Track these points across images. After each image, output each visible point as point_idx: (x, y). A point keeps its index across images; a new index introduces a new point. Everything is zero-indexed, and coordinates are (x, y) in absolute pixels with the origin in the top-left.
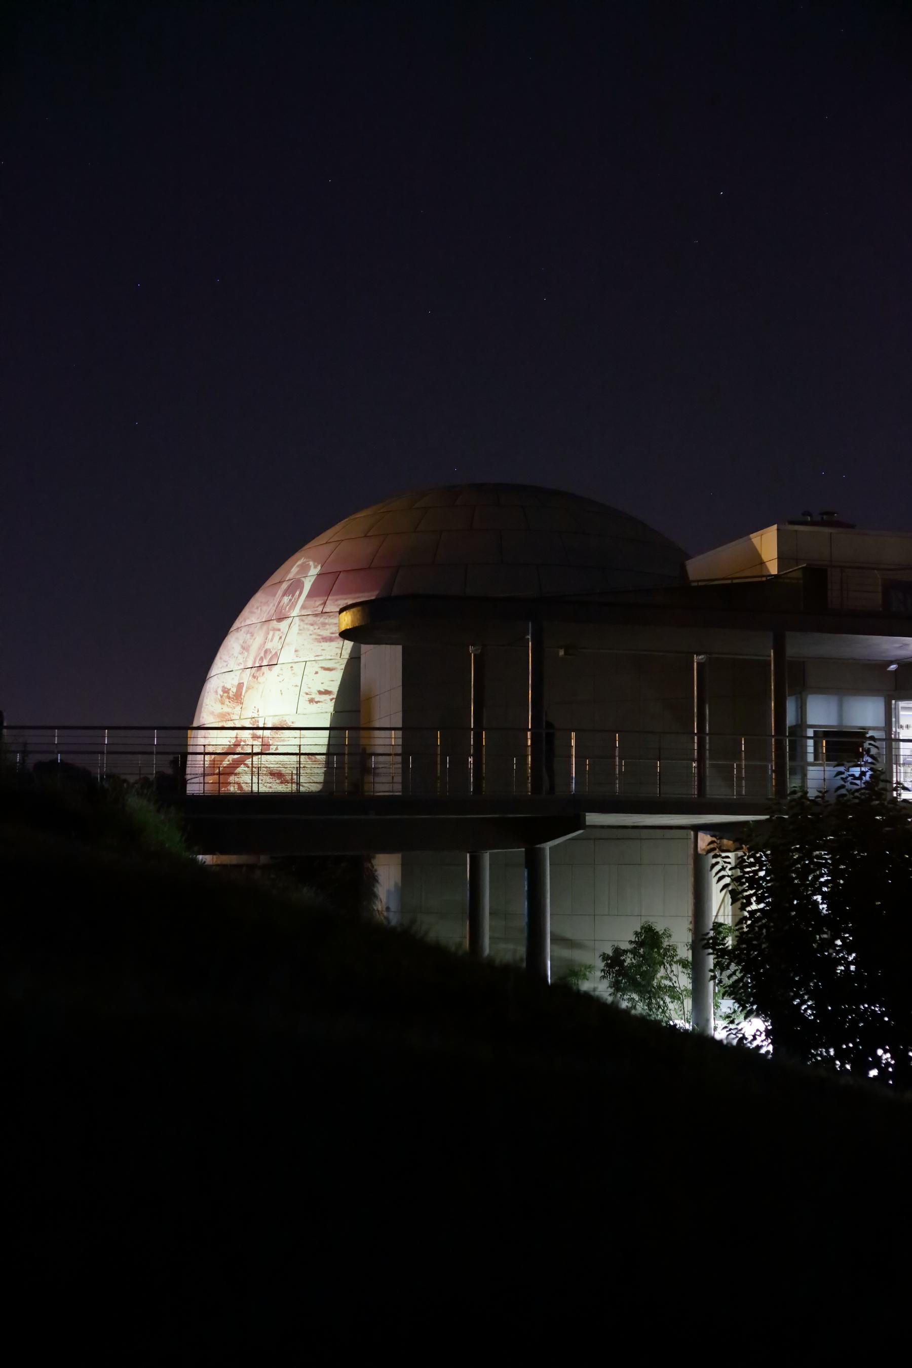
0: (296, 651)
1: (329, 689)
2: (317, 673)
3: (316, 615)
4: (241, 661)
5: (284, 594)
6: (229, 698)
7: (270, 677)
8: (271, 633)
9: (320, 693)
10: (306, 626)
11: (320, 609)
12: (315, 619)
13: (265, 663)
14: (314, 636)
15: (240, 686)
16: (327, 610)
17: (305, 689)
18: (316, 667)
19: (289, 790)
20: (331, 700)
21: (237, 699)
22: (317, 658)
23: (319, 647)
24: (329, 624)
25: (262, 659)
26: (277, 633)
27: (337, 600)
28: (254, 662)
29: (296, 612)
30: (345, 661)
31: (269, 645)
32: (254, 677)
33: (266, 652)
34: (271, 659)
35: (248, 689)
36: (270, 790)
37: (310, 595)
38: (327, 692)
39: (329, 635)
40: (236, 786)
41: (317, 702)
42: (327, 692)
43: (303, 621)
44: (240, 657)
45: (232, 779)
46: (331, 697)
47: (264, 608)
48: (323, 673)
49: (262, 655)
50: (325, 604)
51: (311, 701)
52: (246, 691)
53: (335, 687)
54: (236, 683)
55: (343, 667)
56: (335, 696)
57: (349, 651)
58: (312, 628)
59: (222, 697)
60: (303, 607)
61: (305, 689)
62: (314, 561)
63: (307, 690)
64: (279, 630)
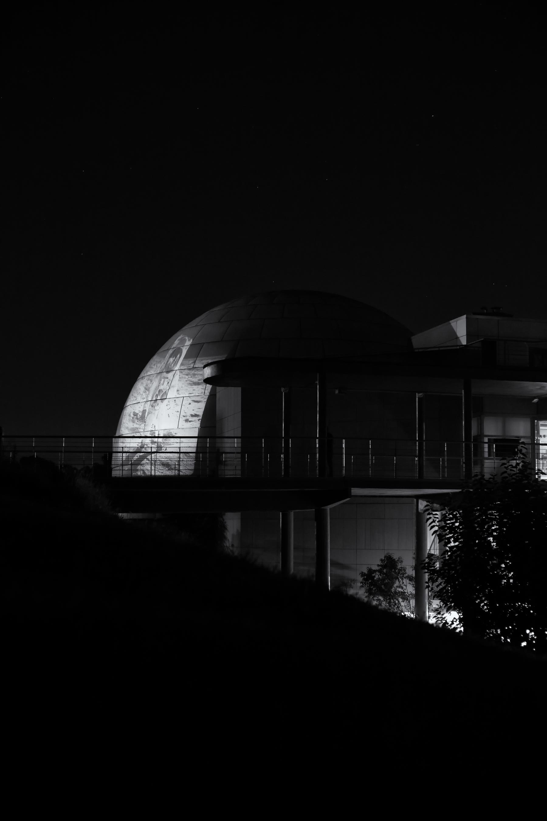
0: (178, 391)
1: (198, 413)
2: (190, 404)
3: (189, 369)
4: (145, 397)
5: (170, 357)
6: (137, 419)
7: (162, 407)
8: (163, 380)
9: (192, 416)
10: (183, 376)
11: (192, 365)
12: (189, 371)
13: (159, 398)
14: (188, 382)
15: (144, 411)
16: (195, 366)
17: (183, 413)
18: (190, 401)
19: (173, 474)
20: (199, 420)
21: (142, 419)
22: (190, 395)
23: (191, 389)
24: (198, 375)
25: (157, 396)
26: (166, 380)
27: (202, 360)
28: (153, 398)
29: (177, 367)
30: (207, 397)
31: (161, 387)
32: (152, 406)
33: (159, 391)
34: (162, 396)
35: (149, 413)
36: (162, 474)
37: (186, 357)
38: (196, 415)
39: (197, 381)
40: (142, 472)
41: (190, 421)
42: (196, 415)
43: (182, 372)
44: (144, 394)
45: (139, 467)
46: (199, 418)
47: (159, 365)
48: (194, 404)
49: (157, 393)
50: (195, 362)
51: (187, 421)
52: (148, 415)
53: (201, 413)
54: (141, 409)
55: (206, 400)
56: (201, 418)
57: (209, 390)
58: (187, 377)
59: (133, 418)
60: (182, 364)
61: (183, 413)
62: (188, 337)
63: (184, 414)
64: (167, 378)
